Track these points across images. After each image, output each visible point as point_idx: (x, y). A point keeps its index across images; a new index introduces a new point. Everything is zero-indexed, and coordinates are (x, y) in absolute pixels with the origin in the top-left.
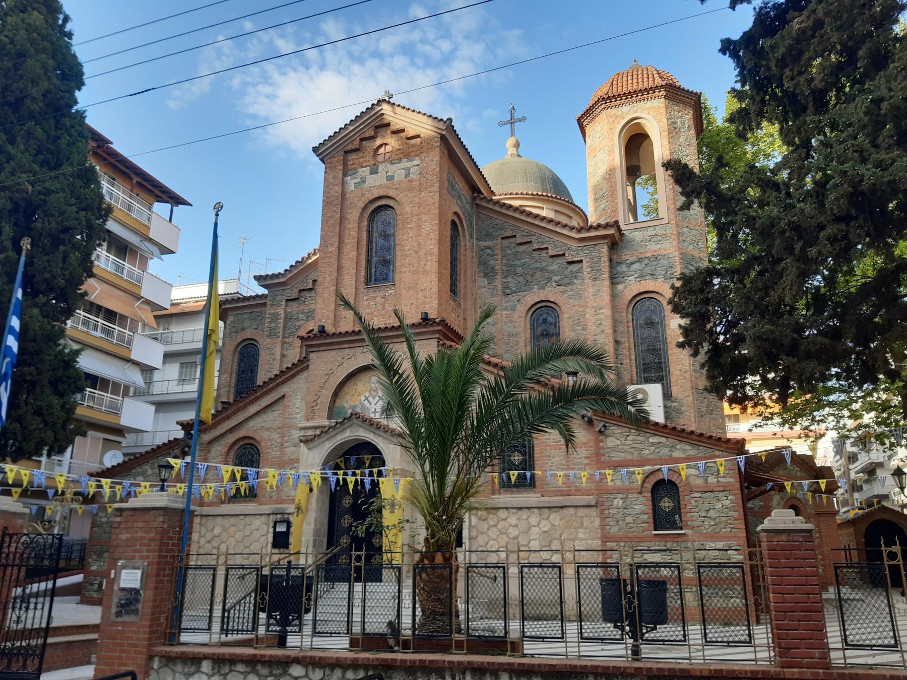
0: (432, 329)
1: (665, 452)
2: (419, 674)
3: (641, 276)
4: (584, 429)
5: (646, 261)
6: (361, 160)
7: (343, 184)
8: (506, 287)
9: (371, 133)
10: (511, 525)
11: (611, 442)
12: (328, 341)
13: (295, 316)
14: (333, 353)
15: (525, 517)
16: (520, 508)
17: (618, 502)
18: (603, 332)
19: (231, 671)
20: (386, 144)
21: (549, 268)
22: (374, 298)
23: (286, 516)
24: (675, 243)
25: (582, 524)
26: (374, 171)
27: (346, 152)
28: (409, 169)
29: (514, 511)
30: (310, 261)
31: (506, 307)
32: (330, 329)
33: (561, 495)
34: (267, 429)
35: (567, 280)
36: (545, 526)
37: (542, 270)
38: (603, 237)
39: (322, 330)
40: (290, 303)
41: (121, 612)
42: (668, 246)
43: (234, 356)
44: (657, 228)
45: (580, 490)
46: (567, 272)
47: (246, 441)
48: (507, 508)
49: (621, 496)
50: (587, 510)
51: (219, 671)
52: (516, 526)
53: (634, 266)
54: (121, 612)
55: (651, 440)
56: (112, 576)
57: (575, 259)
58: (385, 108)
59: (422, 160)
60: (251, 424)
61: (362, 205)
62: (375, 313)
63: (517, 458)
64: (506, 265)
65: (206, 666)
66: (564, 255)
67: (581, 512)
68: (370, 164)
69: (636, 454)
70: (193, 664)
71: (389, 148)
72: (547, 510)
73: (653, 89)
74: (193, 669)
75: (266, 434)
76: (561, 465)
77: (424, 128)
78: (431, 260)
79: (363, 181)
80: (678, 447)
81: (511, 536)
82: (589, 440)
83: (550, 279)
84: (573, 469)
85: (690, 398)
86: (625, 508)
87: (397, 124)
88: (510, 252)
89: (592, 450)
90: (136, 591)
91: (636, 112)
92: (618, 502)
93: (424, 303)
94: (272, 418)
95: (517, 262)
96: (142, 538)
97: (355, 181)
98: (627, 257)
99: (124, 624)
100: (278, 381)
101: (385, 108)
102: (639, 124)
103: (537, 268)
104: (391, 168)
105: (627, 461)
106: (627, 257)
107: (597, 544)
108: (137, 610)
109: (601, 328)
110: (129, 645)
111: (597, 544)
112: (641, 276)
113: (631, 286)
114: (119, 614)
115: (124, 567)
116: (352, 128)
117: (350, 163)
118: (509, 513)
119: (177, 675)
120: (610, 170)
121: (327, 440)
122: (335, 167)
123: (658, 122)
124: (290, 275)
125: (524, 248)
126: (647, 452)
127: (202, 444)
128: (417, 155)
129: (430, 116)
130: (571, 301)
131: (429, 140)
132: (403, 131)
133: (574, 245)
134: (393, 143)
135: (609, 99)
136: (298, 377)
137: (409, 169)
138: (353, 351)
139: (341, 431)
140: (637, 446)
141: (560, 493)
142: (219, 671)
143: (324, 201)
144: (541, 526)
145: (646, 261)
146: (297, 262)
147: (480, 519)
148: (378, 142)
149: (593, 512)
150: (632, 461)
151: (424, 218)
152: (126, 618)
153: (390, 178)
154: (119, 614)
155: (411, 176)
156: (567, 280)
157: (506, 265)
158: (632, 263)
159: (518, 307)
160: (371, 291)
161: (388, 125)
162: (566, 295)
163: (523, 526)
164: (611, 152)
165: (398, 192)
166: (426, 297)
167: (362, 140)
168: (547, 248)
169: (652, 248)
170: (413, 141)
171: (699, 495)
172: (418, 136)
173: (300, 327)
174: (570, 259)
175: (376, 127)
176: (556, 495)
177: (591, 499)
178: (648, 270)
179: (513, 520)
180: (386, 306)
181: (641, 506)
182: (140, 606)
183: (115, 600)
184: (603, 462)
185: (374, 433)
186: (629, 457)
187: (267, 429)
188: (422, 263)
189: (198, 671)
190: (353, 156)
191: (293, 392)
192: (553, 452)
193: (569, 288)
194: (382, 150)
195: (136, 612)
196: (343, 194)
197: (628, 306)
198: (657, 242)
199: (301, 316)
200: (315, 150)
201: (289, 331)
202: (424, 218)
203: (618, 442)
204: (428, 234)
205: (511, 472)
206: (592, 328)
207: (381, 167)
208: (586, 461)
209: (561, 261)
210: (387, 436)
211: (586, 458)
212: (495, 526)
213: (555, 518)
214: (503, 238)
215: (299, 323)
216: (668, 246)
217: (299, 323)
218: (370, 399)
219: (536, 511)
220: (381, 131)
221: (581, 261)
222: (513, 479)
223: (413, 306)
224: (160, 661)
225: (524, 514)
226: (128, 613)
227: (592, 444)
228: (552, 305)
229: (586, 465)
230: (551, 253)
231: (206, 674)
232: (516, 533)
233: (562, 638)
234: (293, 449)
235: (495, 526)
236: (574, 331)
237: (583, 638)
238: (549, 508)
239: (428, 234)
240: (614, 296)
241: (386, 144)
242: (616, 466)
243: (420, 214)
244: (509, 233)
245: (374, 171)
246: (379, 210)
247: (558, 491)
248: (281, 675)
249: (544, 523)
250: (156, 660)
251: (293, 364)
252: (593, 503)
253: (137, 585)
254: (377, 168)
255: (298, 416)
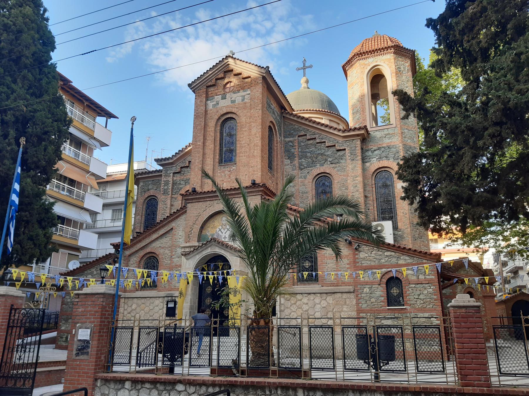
0: (257, 189)
1: (394, 260)
2: (251, 390)
3: (380, 158)
4: (346, 248)
5: (383, 149)
6: (216, 91)
7: (206, 105)
8: (300, 164)
9: (221, 75)
10: (304, 303)
11: (362, 255)
12: (198, 197)
13: (179, 182)
14: (200, 203)
15: (312, 298)
16: (310, 294)
17: (366, 290)
18: (357, 191)
19: (142, 387)
20: (231, 82)
21: (326, 154)
22: (224, 172)
23: (174, 298)
24: (400, 139)
25: (345, 302)
26: (224, 98)
27: (208, 87)
28: (244, 96)
29: (306, 295)
30: (187, 150)
31: (301, 177)
32: (198, 190)
33: (333, 286)
34: (163, 248)
35: (336, 161)
36: (324, 304)
37: (322, 154)
38: (358, 135)
39: (194, 190)
40: (175, 175)
41: (78, 353)
42: (396, 140)
43: (143, 205)
44: (389, 130)
45: (344, 283)
46: (336, 156)
47: (151, 255)
48: (301, 294)
49: (368, 286)
50: (348, 295)
51: (135, 388)
52: (307, 304)
53: (376, 152)
54: (78, 353)
55: (386, 254)
56: (74, 333)
57: (341, 148)
58: (230, 61)
59: (251, 91)
60: (154, 245)
61: (217, 118)
62: (225, 180)
63: (307, 264)
64: (301, 152)
65: (128, 385)
66: (335, 146)
67: (345, 296)
68: (221, 93)
69: (377, 262)
70: (120, 383)
71: (232, 84)
72: (325, 295)
73: (387, 48)
74: (120, 386)
75: (162, 251)
76: (333, 268)
77: (253, 72)
78: (257, 149)
79: (218, 104)
80: (402, 258)
81: (304, 310)
82: (349, 254)
83: (326, 160)
84: (340, 270)
85: (409, 229)
86: (370, 294)
87: (237, 70)
88: (303, 144)
89: (352, 260)
90: (88, 342)
91: (377, 62)
92: (366, 290)
93: (253, 174)
94: (165, 241)
95: (307, 150)
96: (90, 311)
97: (213, 103)
98: (372, 147)
99: (81, 360)
100: (168, 220)
101: (230, 61)
102: (378, 69)
103: (319, 154)
104: (234, 96)
105: (372, 266)
106: (372, 147)
107: (354, 314)
108: (88, 352)
109: (357, 188)
110: (83, 373)
111: (354, 314)
112: (380, 158)
113: (374, 164)
114: (77, 355)
115: (80, 328)
116: (211, 73)
117: (210, 93)
118: (303, 296)
119: (111, 390)
120: (362, 96)
121: (197, 254)
122: (201, 95)
123: (390, 67)
124: (175, 159)
125: (311, 142)
126: (383, 261)
127: (125, 257)
128: (248, 88)
129: (256, 65)
130: (339, 173)
131: (256, 79)
132: (240, 74)
133: (341, 140)
134: (235, 81)
135: (360, 54)
136: (181, 217)
137: (244, 96)
138: (212, 202)
139: (205, 249)
140: (378, 257)
141: (332, 285)
142: (135, 388)
143: (195, 115)
144: (322, 303)
145: (383, 149)
146: (179, 151)
147: (286, 299)
148: (226, 80)
149: (352, 296)
150: (374, 266)
151: (253, 125)
152: (81, 357)
153: (233, 102)
154: (77, 355)
155: (245, 100)
156: (336, 161)
157: (301, 152)
158: (375, 150)
159: (308, 176)
160: (222, 167)
161: (232, 70)
162: (336, 169)
163: (311, 304)
164: (362, 85)
165: (238, 110)
166: (254, 171)
167: (217, 79)
168: (325, 142)
169: (386, 142)
170: (246, 80)
171: (414, 286)
172: (249, 77)
173: (181, 188)
174: (338, 148)
175: (225, 72)
176: (331, 286)
177: (351, 288)
178: (384, 154)
179: (305, 300)
180: (231, 176)
181: (380, 292)
182: (89, 350)
183: (75, 347)
184: (358, 267)
185: (225, 250)
186: (373, 264)
187: (163, 248)
188: (252, 151)
189: (123, 387)
190: (212, 89)
191: (178, 226)
192: (329, 261)
193: (338, 165)
194: (228, 85)
195: (87, 353)
196: (206, 111)
197: (372, 175)
198: (389, 138)
199: (182, 182)
200: (189, 85)
201: (175, 191)
202: (253, 125)
203: (367, 255)
204: (255, 134)
205: (304, 273)
206: (351, 188)
207: (228, 95)
208: (348, 266)
209: (333, 149)
210: (233, 252)
211: (348, 264)
212: (295, 304)
213: (330, 299)
214: (299, 136)
215: (181, 186)
216: (396, 140)
217: (181, 186)
218: (222, 230)
219: (319, 295)
220: (228, 75)
221: (345, 149)
222: (305, 276)
223: (247, 176)
224: (101, 382)
225: (312, 297)
226: (83, 354)
227: (351, 256)
228: (328, 175)
229: (348, 268)
230: (327, 145)
231: (128, 390)
232: (307, 308)
233: (334, 369)
234: (177, 259)
235: (295, 304)
236: (341, 190)
237: (419, 371)
238: (326, 293)
239: (255, 134)
240: (364, 170)
241: (231, 82)
242: (365, 269)
243: (251, 122)
244: (303, 133)
245: (224, 98)
246: (227, 120)
247: (331, 283)
248: (171, 390)
249: (323, 302)
250: (99, 381)
251: (177, 210)
252: (352, 291)
253: (88, 338)
254: (226, 96)
255: (180, 240)
